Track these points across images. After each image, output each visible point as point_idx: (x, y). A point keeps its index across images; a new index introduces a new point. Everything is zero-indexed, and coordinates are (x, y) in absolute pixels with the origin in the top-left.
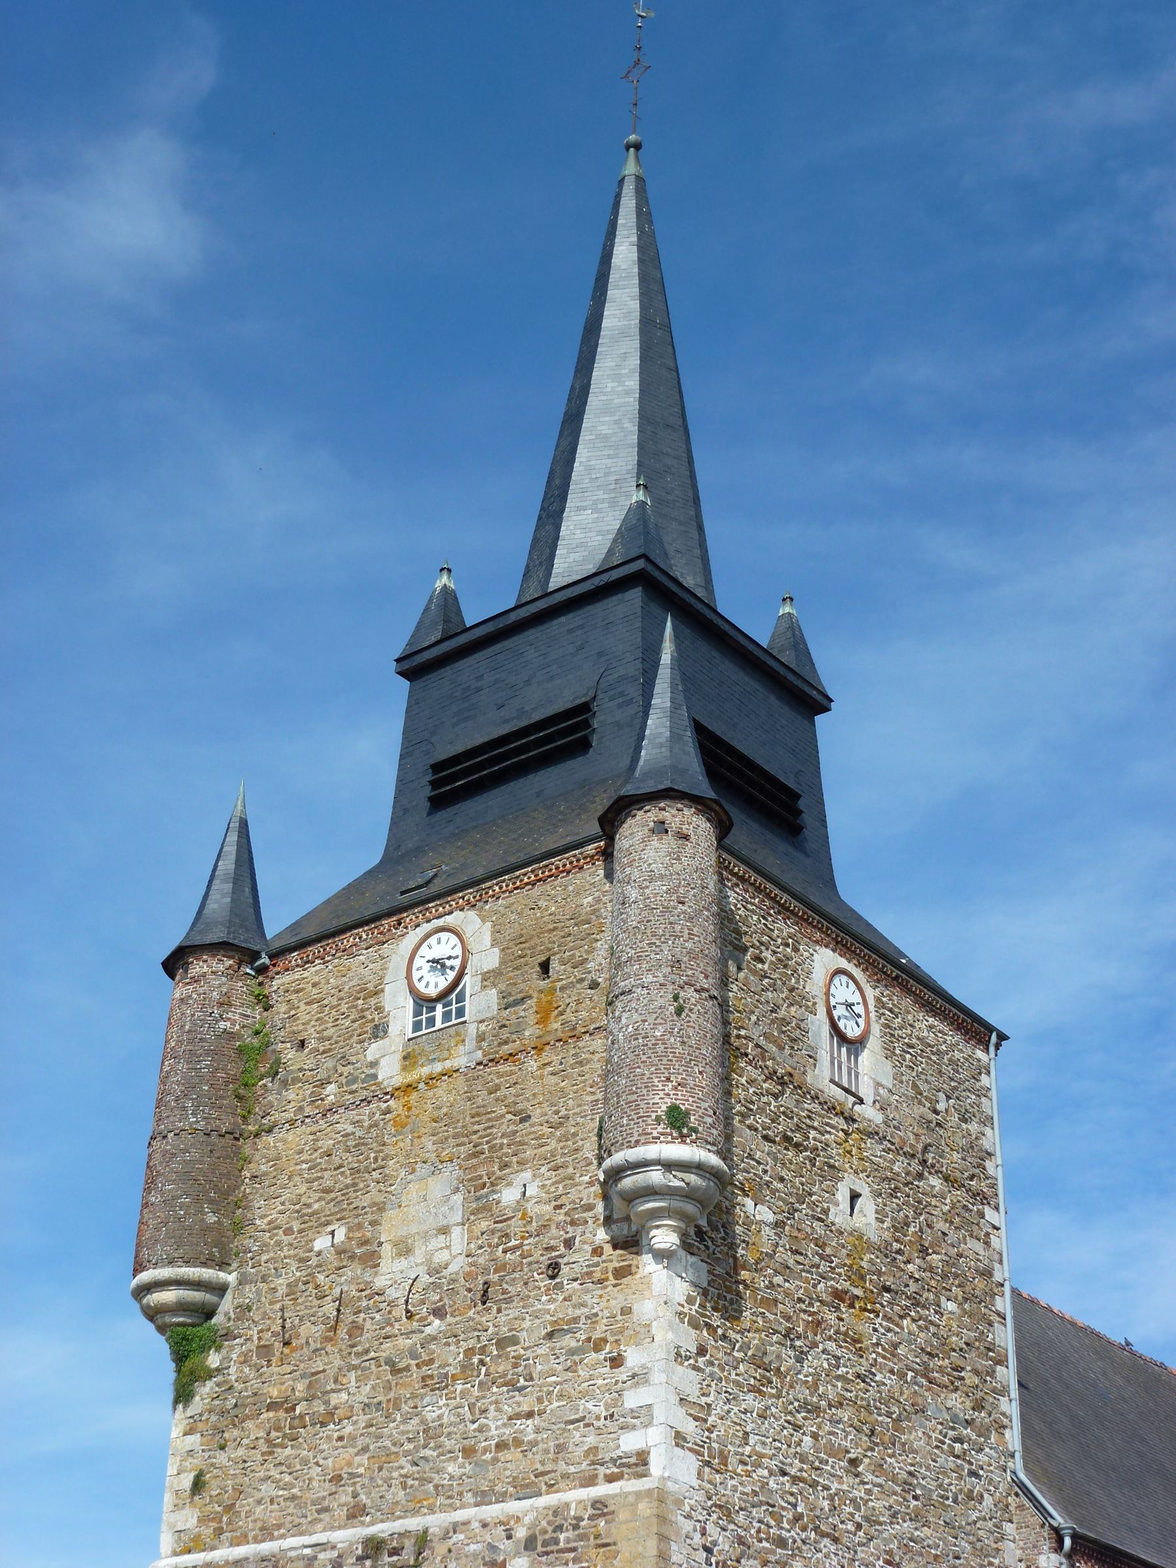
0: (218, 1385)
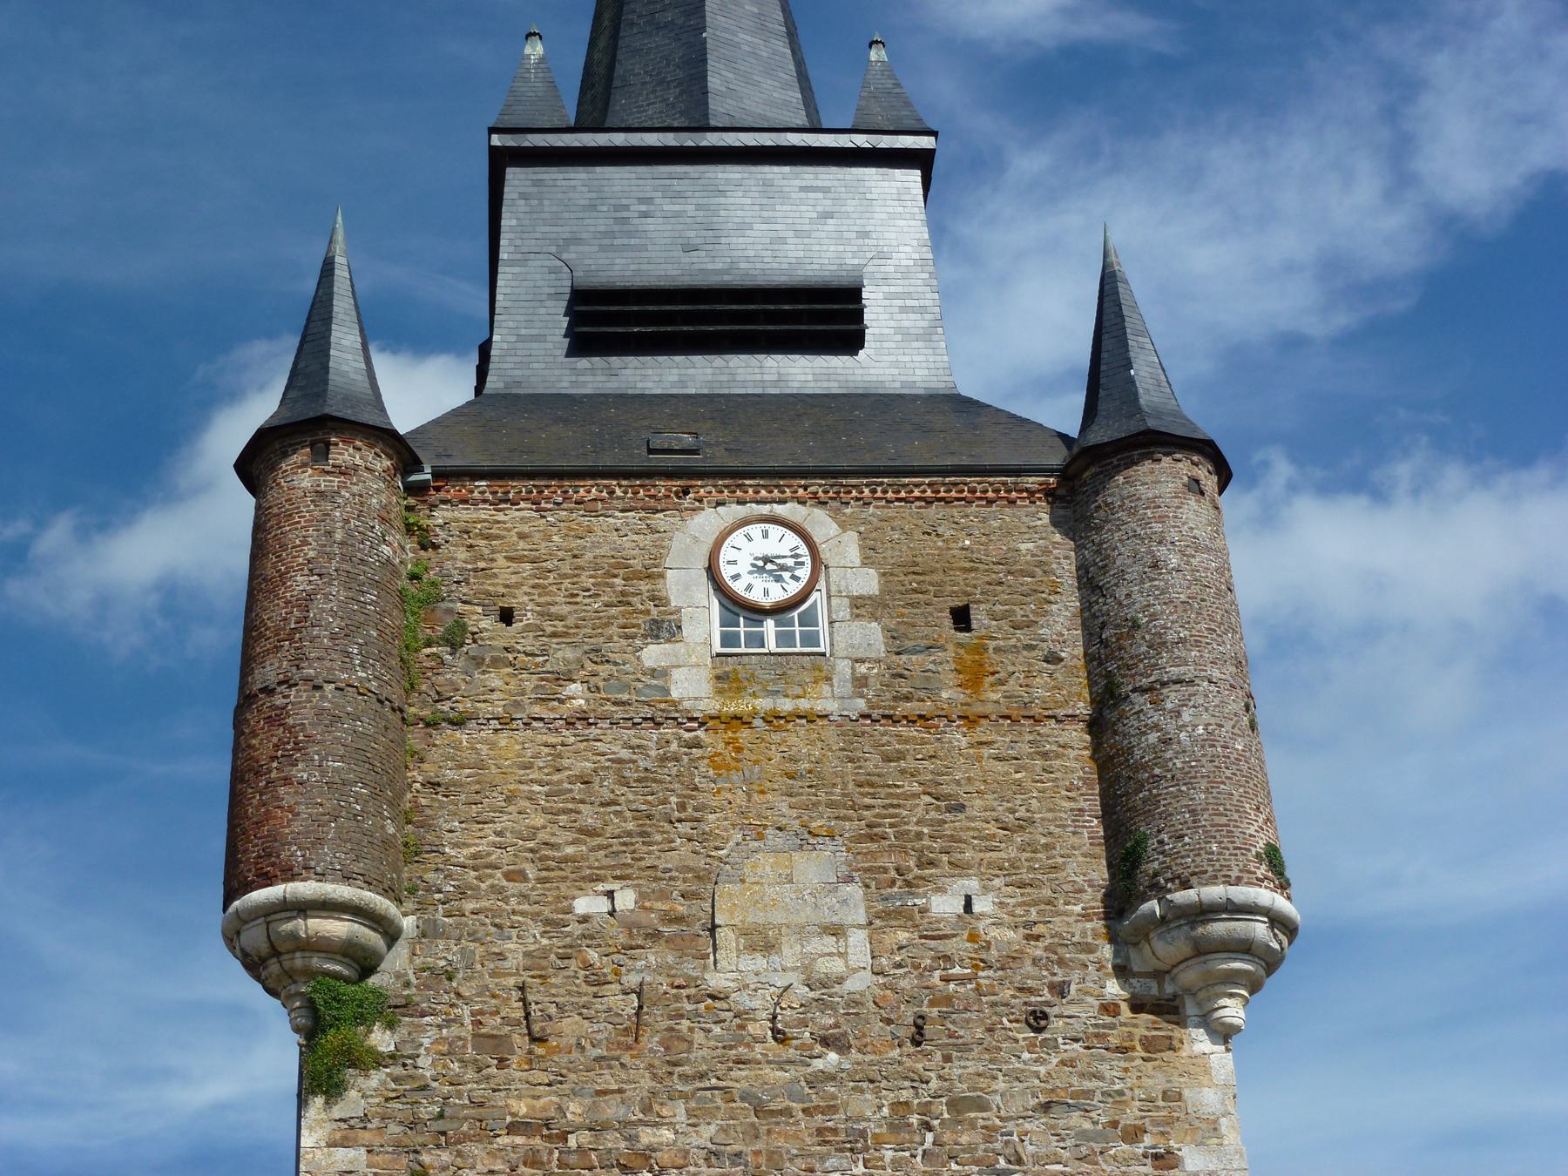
0: (395, 1080)
